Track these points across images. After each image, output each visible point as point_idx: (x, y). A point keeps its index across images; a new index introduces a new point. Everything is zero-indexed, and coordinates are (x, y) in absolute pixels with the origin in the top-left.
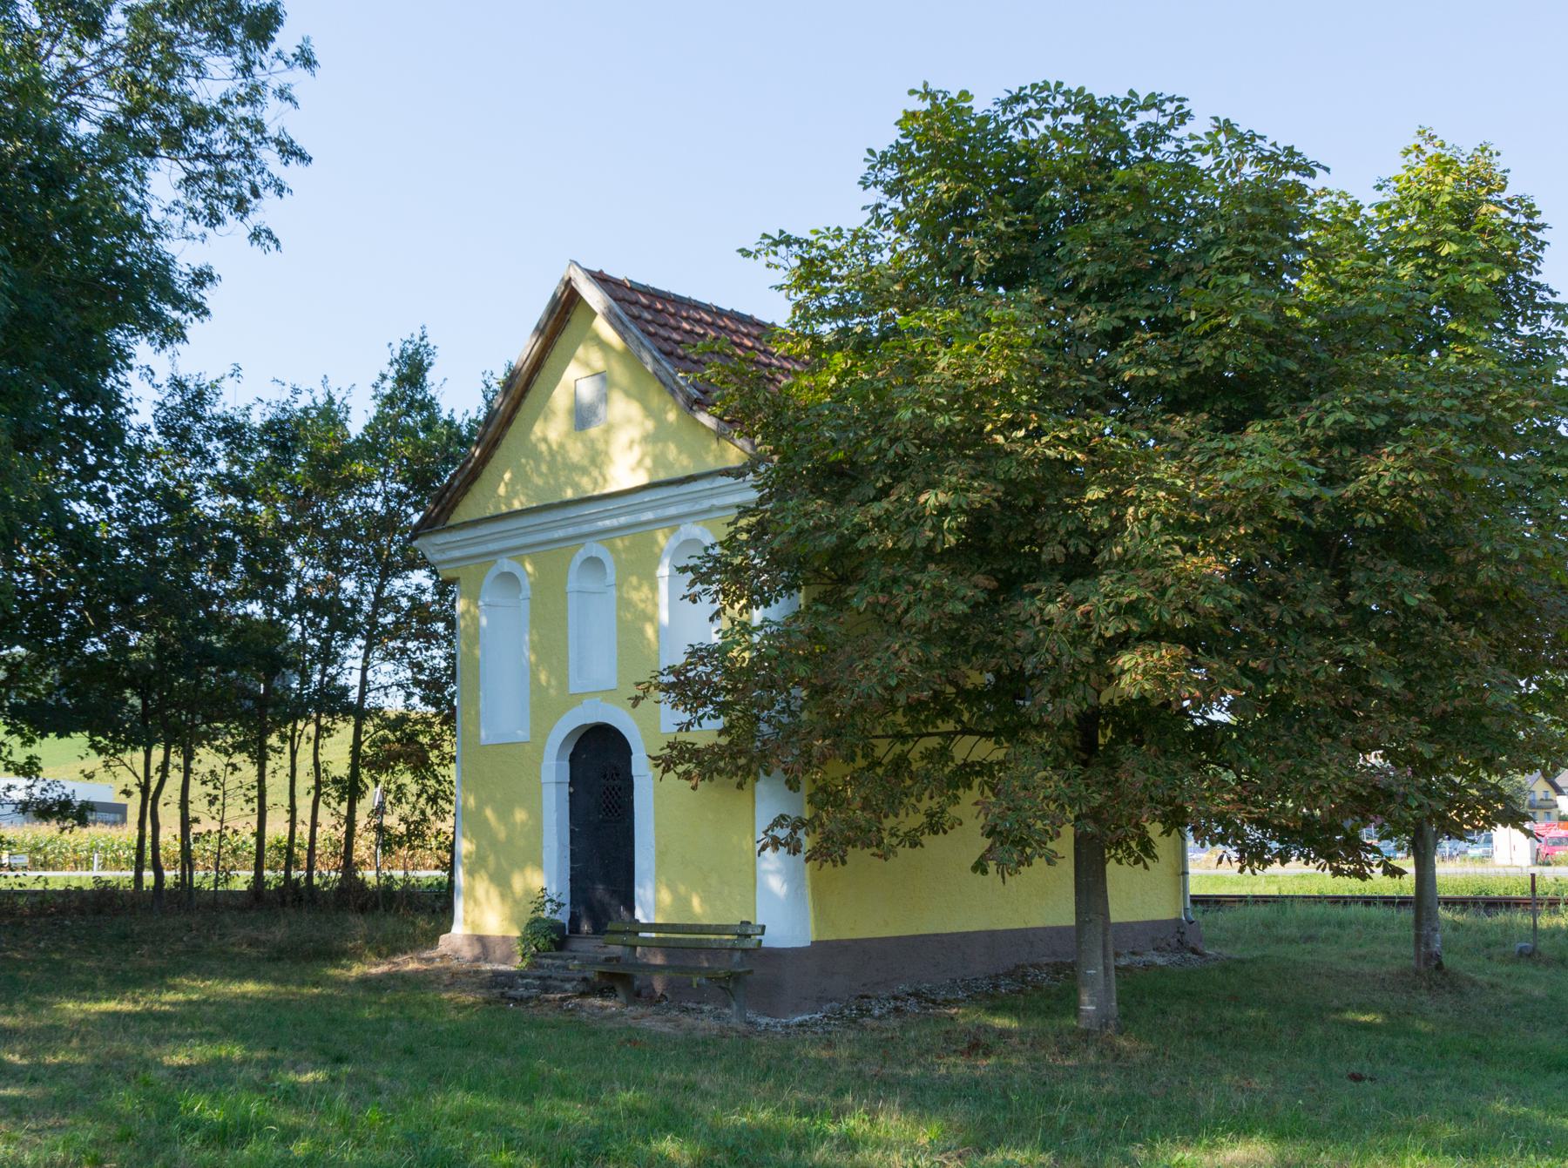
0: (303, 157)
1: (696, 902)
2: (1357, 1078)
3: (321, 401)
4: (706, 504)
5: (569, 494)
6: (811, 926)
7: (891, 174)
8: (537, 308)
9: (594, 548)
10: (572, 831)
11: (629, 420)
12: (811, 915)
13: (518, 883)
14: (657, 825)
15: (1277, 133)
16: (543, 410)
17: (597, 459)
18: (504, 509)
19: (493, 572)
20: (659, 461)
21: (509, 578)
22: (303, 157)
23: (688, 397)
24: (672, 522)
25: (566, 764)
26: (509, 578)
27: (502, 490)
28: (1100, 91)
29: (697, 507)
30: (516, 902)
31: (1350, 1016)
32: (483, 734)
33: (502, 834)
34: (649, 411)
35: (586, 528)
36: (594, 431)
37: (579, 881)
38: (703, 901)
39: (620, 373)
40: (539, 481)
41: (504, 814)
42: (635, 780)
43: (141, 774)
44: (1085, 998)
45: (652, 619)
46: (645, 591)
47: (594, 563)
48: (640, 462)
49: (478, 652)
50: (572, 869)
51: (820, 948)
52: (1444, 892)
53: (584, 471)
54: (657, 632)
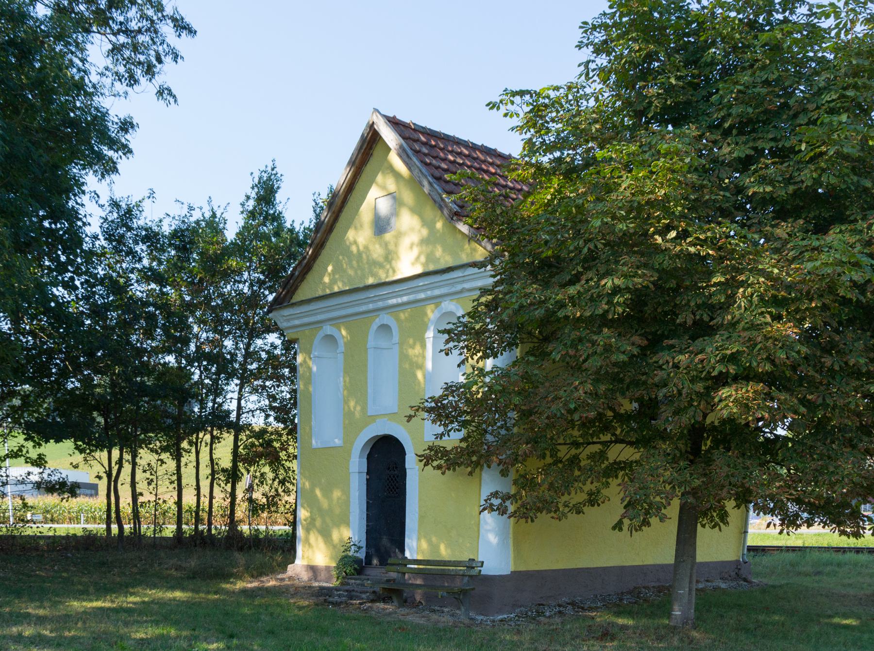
3: (208, 215)
4: (459, 287)
5: (371, 281)
6: (511, 562)
7: (599, 37)
9: (386, 318)
10: (368, 503)
12: (512, 555)
13: (335, 536)
14: (420, 500)
17: (390, 257)
18: (328, 292)
20: (430, 258)
22: (191, 32)
24: (436, 300)
25: (365, 460)
27: (326, 279)
29: (453, 290)
30: (334, 547)
31: (836, 620)
33: (325, 504)
35: (380, 304)
36: (388, 236)
37: (372, 533)
38: (446, 547)
40: (351, 272)
41: (327, 493)
43: (106, 464)
44: (676, 607)
45: (421, 367)
46: (417, 350)
47: (385, 328)
50: (367, 526)
53: (381, 266)
54: (425, 376)
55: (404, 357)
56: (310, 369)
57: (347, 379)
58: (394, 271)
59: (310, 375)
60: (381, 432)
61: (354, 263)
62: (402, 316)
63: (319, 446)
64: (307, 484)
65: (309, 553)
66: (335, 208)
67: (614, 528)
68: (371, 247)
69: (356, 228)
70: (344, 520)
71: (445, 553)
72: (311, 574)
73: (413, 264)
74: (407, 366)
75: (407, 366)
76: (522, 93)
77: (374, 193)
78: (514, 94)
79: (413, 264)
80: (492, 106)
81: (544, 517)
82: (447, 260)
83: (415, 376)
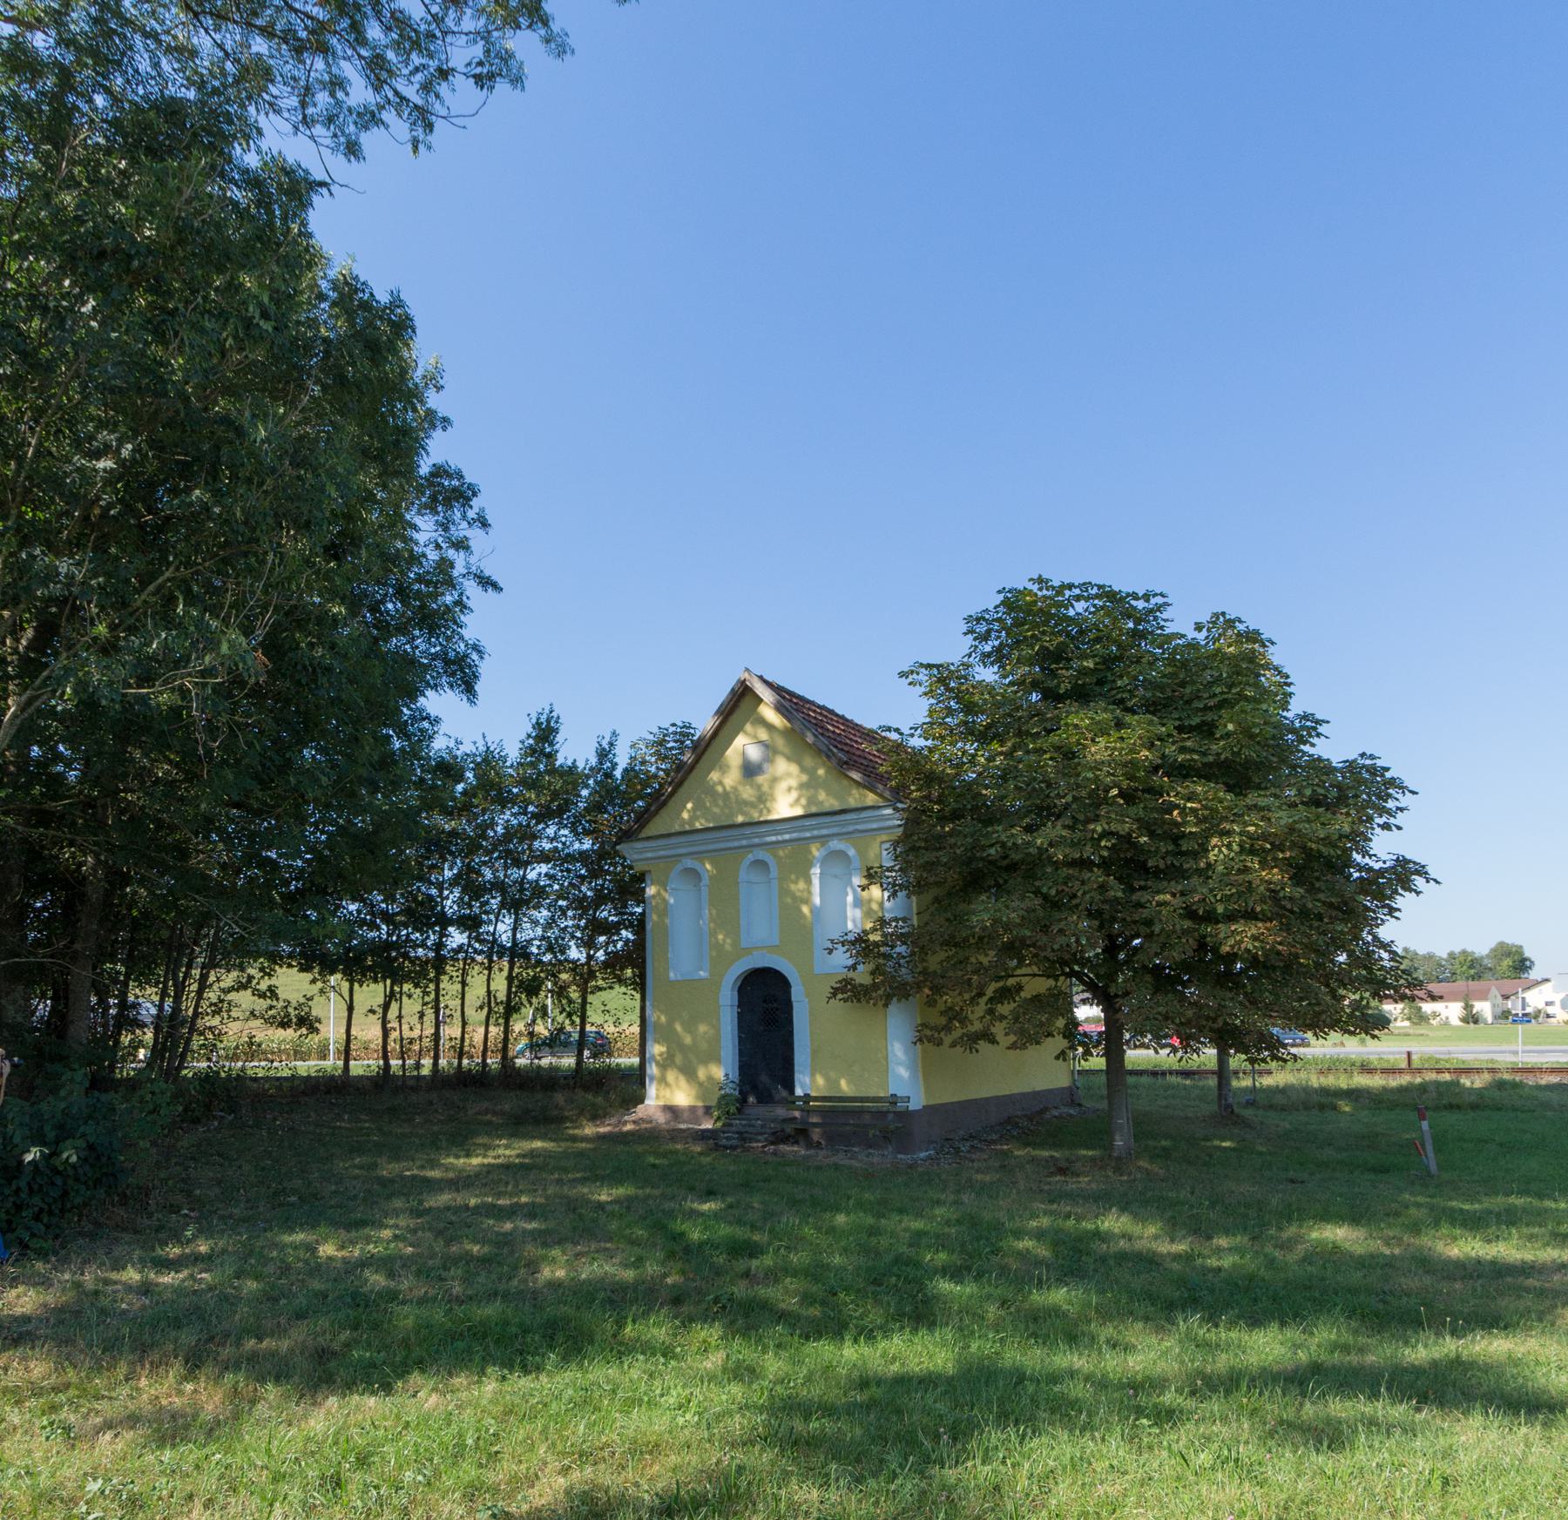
0: (495, 586)
1: (843, 1084)
2: (1293, 1181)
3: (482, 748)
4: (851, 828)
5: (740, 819)
6: (923, 1096)
7: (982, 628)
8: (721, 694)
9: (761, 854)
10: (740, 1037)
11: (789, 775)
12: (923, 1090)
13: (702, 1074)
15: (1252, 622)
16: (719, 763)
17: (763, 799)
18: (687, 828)
19: (679, 867)
20: (811, 801)
21: (694, 874)
22: (495, 586)
23: (840, 759)
26: (694, 874)
27: (685, 815)
28: (1122, 585)
29: (845, 830)
30: (701, 1084)
31: (1216, 1143)
32: (672, 975)
33: (688, 1040)
34: (803, 769)
35: (756, 841)
36: (760, 779)
37: (747, 1068)
38: (848, 1083)
39: (780, 742)
40: (716, 810)
41: (690, 1028)
42: (795, 1005)
43: (347, 998)
44: (1117, 1137)
45: (807, 901)
46: (801, 885)
48: (797, 801)
49: (667, 921)
51: (929, 1110)
52: (1129, 1066)
53: (753, 805)
54: (811, 911)
55: (785, 892)
56: (665, 900)
57: (714, 912)
58: (769, 811)
59: (666, 907)
60: (760, 965)
61: (720, 802)
62: (781, 853)
63: (679, 978)
64: (663, 1018)
65: (667, 1093)
66: (699, 750)
67: (1057, 1058)
68: (740, 788)
69: (721, 768)
70: (713, 1057)
71: (845, 1087)
72: (669, 1116)
73: (792, 806)
74: (789, 900)
75: (789, 900)
76: (929, 666)
77: (740, 741)
78: (922, 665)
79: (792, 806)
80: (903, 675)
81: (1426, 1057)
82: (831, 803)
83: (800, 910)
